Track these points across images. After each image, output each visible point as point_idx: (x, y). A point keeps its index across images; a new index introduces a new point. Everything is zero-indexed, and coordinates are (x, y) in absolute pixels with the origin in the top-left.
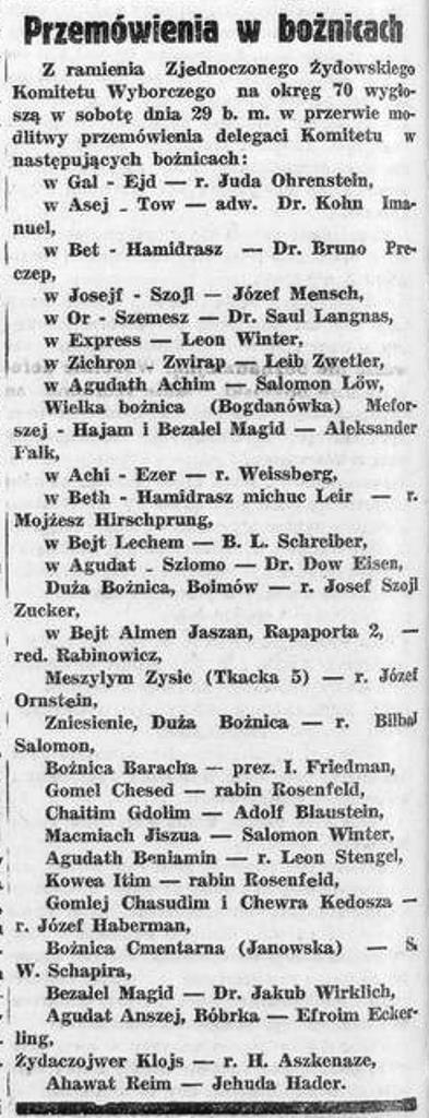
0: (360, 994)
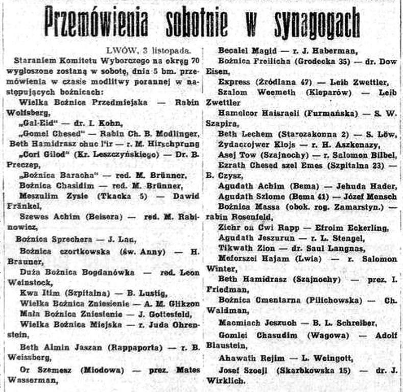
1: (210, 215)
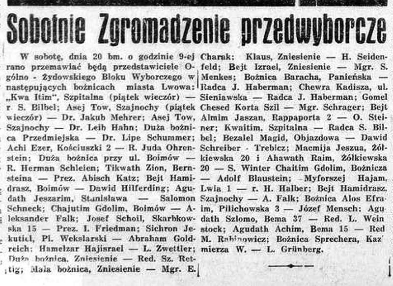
0: (359, 159)
1: (300, 75)
